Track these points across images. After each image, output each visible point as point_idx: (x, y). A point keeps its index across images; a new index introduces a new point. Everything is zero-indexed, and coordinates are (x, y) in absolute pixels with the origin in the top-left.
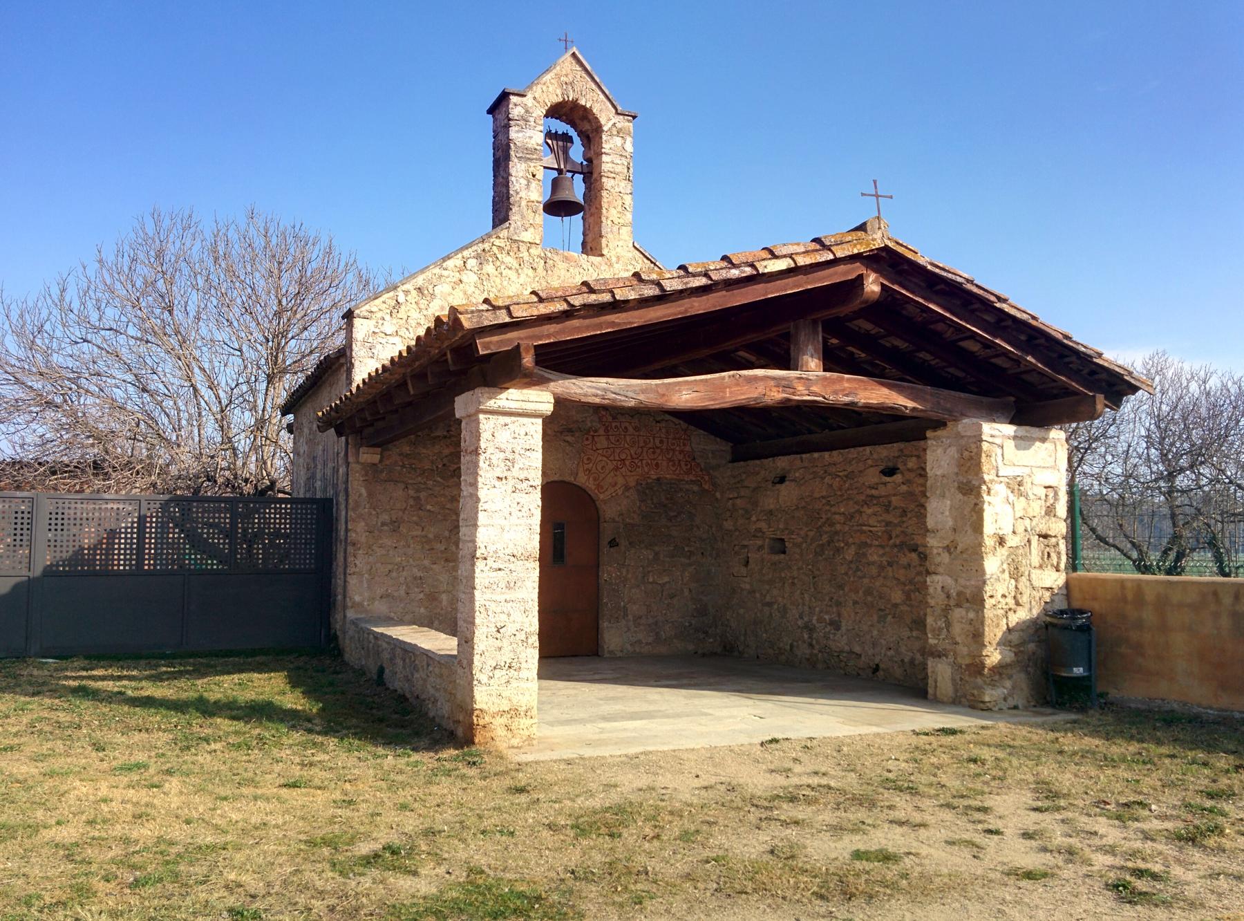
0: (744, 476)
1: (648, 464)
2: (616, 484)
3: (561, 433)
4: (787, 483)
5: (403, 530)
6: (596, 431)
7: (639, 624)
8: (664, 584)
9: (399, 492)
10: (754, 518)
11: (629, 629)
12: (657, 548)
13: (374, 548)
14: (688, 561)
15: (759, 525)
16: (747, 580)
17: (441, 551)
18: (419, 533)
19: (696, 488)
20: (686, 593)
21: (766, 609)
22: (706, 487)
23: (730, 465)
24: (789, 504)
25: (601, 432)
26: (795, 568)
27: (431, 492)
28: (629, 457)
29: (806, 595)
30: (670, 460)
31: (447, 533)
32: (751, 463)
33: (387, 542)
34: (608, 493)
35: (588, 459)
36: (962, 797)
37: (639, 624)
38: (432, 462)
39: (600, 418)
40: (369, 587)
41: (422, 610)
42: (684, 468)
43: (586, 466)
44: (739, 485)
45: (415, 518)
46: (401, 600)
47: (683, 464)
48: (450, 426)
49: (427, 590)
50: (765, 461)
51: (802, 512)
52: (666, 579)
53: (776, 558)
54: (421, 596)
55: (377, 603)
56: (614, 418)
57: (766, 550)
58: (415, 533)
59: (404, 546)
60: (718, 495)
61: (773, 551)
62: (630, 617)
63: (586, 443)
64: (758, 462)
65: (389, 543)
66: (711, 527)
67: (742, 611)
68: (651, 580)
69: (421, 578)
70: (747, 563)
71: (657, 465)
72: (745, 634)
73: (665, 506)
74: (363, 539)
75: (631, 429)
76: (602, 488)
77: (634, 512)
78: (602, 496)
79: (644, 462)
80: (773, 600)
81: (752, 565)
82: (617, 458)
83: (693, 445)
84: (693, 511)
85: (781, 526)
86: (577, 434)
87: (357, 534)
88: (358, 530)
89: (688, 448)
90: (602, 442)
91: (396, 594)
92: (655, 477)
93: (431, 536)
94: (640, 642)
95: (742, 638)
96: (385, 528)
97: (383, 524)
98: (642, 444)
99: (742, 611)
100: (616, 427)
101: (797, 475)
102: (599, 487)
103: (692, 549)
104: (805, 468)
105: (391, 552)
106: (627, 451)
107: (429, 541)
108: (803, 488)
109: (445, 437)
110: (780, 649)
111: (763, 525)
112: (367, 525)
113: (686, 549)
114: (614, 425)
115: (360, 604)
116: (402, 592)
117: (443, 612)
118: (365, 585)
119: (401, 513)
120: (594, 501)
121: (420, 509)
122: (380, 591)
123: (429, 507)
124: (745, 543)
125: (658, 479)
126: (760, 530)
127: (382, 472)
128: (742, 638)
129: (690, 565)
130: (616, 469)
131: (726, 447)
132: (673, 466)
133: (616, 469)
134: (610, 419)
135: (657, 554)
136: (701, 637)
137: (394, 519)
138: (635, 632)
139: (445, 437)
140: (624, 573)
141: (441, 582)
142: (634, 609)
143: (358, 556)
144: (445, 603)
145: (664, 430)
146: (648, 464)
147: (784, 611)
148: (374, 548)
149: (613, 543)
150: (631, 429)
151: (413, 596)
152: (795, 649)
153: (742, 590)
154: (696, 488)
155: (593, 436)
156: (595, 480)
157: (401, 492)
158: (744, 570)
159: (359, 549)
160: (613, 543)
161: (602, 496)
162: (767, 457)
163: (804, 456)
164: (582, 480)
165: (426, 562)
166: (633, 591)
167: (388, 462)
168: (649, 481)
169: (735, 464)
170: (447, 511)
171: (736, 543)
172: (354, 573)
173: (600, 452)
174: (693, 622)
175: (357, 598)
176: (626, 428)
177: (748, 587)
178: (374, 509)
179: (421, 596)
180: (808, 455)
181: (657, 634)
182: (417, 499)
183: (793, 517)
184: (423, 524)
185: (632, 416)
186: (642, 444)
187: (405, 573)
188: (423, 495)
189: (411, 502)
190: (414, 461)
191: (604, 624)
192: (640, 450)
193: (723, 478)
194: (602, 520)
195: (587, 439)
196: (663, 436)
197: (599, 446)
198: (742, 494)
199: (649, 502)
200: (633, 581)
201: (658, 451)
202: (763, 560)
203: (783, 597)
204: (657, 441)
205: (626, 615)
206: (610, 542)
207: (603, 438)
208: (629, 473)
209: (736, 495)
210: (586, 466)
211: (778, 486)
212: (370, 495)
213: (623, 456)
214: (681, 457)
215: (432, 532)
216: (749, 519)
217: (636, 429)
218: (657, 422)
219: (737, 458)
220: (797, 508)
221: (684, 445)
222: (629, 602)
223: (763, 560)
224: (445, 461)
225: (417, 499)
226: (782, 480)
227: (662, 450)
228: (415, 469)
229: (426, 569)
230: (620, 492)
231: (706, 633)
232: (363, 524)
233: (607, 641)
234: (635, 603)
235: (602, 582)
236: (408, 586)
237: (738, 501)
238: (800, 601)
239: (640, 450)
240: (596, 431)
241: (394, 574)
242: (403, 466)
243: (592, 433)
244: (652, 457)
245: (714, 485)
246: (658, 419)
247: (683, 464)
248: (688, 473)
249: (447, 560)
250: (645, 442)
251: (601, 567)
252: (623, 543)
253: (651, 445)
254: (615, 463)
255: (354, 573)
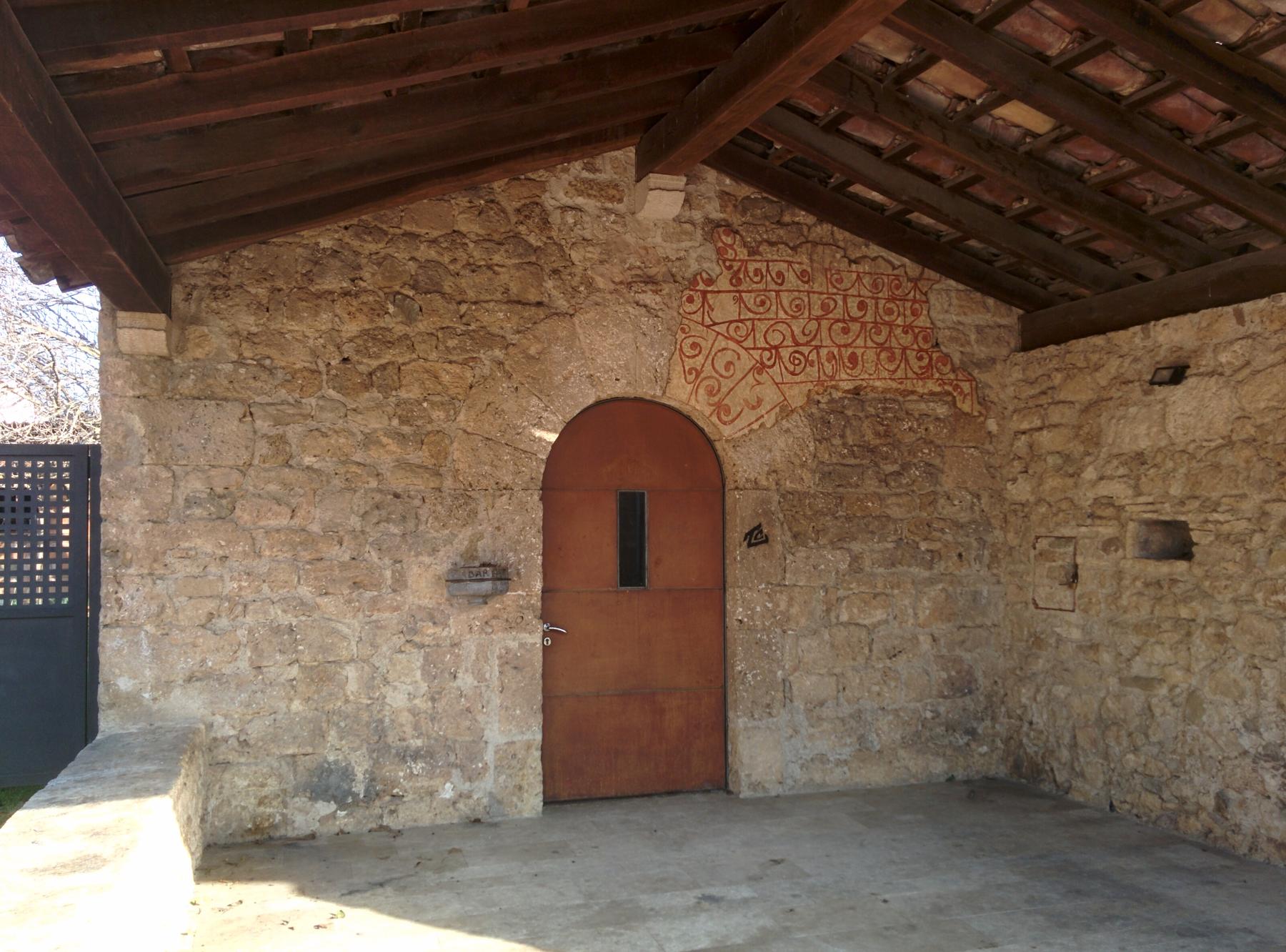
0: (1058, 378)
1: (831, 357)
2: (760, 401)
3: (629, 285)
4: (1191, 382)
5: (244, 515)
6: (710, 282)
7: (820, 719)
8: (875, 626)
9: (228, 424)
10: (1090, 474)
11: (796, 732)
12: (856, 547)
13: (169, 559)
14: (927, 574)
15: (1105, 489)
16: (1073, 617)
17: (343, 566)
18: (284, 522)
19: (942, 410)
20: (925, 644)
21: (1136, 697)
22: (966, 407)
23: (1020, 357)
24: (1200, 433)
25: (723, 283)
26: (1229, 595)
27: (313, 424)
28: (789, 342)
29: (1267, 672)
30: (881, 347)
31: (355, 522)
32: (1079, 345)
33: (205, 545)
34: (740, 423)
35: (694, 345)
36: (1228, 867)
37: (820, 719)
38: (315, 354)
39: (719, 252)
40: (156, 656)
41: (296, 705)
42: (915, 364)
43: (689, 363)
44: (1044, 400)
45: (272, 487)
46: (239, 686)
47: (911, 355)
48: (359, 267)
49: (306, 659)
50: (1120, 337)
51: (1247, 452)
52: (879, 615)
53: (1163, 569)
54: (294, 671)
55: (177, 692)
56: (753, 252)
57: (1131, 548)
58: (273, 523)
59: (245, 554)
60: (992, 425)
61: (1151, 553)
62: (799, 704)
63: (689, 308)
64: (1098, 340)
65: (209, 548)
66: (978, 497)
67: (1060, 691)
68: (844, 617)
69: (291, 629)
70: (1073, 578)
71: (853, 359)
72: (1074, 746)
73: (873, 450)
74: (138, 539)
75: (791, 278)
76: (728, 411)
77: (803, 465)
78: (727, 431)
79: (824, 352)
80: (1155, 673)
81: (1087, 582)
82: (761, 344)
83: (933, 314)
84: (937, 462)
85: (1176, 490)
86: (666, 288)
87: (121, 526)
88: (125, 518)
89: (922, 321)
90: (725, 308)
91: (227, 670)
92: (848, 386)
93: (315, 528)
94: (822, 758)
95: (1065, 754)
96: (198, 512)
97: (190, 502)
98: (817, 312)
99: (1060, 691)
100: (757, 272)
101: (1224, 358)
102: (720, 408)
103: (936, 546)
104: (1252, 336)
105: (213, 569)
106: (782, 327)
107: (309, 540)
108: (1246, 389)
109: (346, 294)
110: (1183, 801)
111: (1118, 490)
112: (147, 504)
113: (923, 546)
114: (752, 267)
115: (134, 698)
116: (243, 664)
117: (349, 708)
118: (146, 652)
119: (236, 475)
120: (710, 443)
121: (287, 464)
122: (183, 665)
123: (308, 460)
124: (1066, 532)
125: (856, 391)
126: (1110, 502)
127: (184, 375)
128: (1065, 754)
129: (932, 581)
130: (761, 367)
131: (1010, 317)
132: (891, 359)
133: (761, 367)
134: (743, 254)
135: (855, 558)
136: (961, 742)
137: (219, 490)
138: (811, 737)
139: (346, 294)
140: (783, 606)
141: (345, 638)
142: (806, 684)
143: (125, 581)
144: (352, 687)
145: (866, 280)
146: (831, 357)
147: (1192, 705)
148: (169, 559)
149: (756, 537)
150: (791, 278)
151: (271, 672)
152: (1233, 808)
153: (1060, 640)
154: (942, 410)
155: (704, 293)
156: (711, 393)
157: (234, 425)
158: (1064, 596)
159: (128, 565)
160: (756, 537)
161: (727, 431)
162: (1124, 326)
163: (1247, 307)
164: (680, 394)
165: (305, 591)
166: (804, 643)
167: (199, 353)
168: (837, 395)
169: (1036, 353)
170: (354, 468)
171: (1043, 531)
172: (117, 623)
173: (721, 329)
174: (942, 709)
175: (125, 684)
176: (780, 274)
177: (1076, 634)
178: (166, 466)
179: (294, 671)
180: (1262, 303)
181: (861, 738)
182: (279, 442)
183: (1217, 467)
184: (294, 501)
185: (794, 249)
186: (817, 312)
187: (249, 619)
188: (294, 432)
189: (263, 448)
190: (267, 351)
191: (739, 722)
192: (813, 325)
193: (1004, 386)
194: (730, 485)
195: (690, 300)
196: (864, 292)
197: (718, 315)
198: (1055, 419)
199: (837, 441)
200: (803, 621)
201: (855, 327)
202: (1119, 575)
203: (1188, 670)
204: (853, 304)
205: (788, 699)
206: (749, 535)
207: (727, 299)
208: (789, 378)
209: (1038, 423)
210: (689, 363)
211: (1162, 392)
212: (155, 432)
213: (775, 339)
214: (907, 340)
215: (316, 518)
216: (1076, 475)
217: (804, 276)
218: (851, 262)
219: (1030, 342)
220: (1229, 443)
221: (915, 313)
222: (795, 669)
223: (1119, 575)
224: (348, 350)
225: (279, 442)
226: (1177, 374)
227: (864, 324)
228: (271, 371)
229: (303, 606)
230: (769, 420)
231: (972, 733)
232: (137, 502)
233: (746, 760)
234: (808, 672)
235: (731, 623)
236: (256, 648)
237: (1045, 438)
238: (1248, 685)
239: (814, 325)
240: (710, 282)
241: (223, 622)
242: (240, 362)
243: (701, 287)
244: (842, 340)
245: (983, 401)
246: (855, 254)
247: (911, 355)
248: (922, 376)
249: (356, 585)
250: (824, 306)
251: (730, 591)
252: (780, 536)
253: (838, 313)
254: (756, 354)
255: (117, 623)
